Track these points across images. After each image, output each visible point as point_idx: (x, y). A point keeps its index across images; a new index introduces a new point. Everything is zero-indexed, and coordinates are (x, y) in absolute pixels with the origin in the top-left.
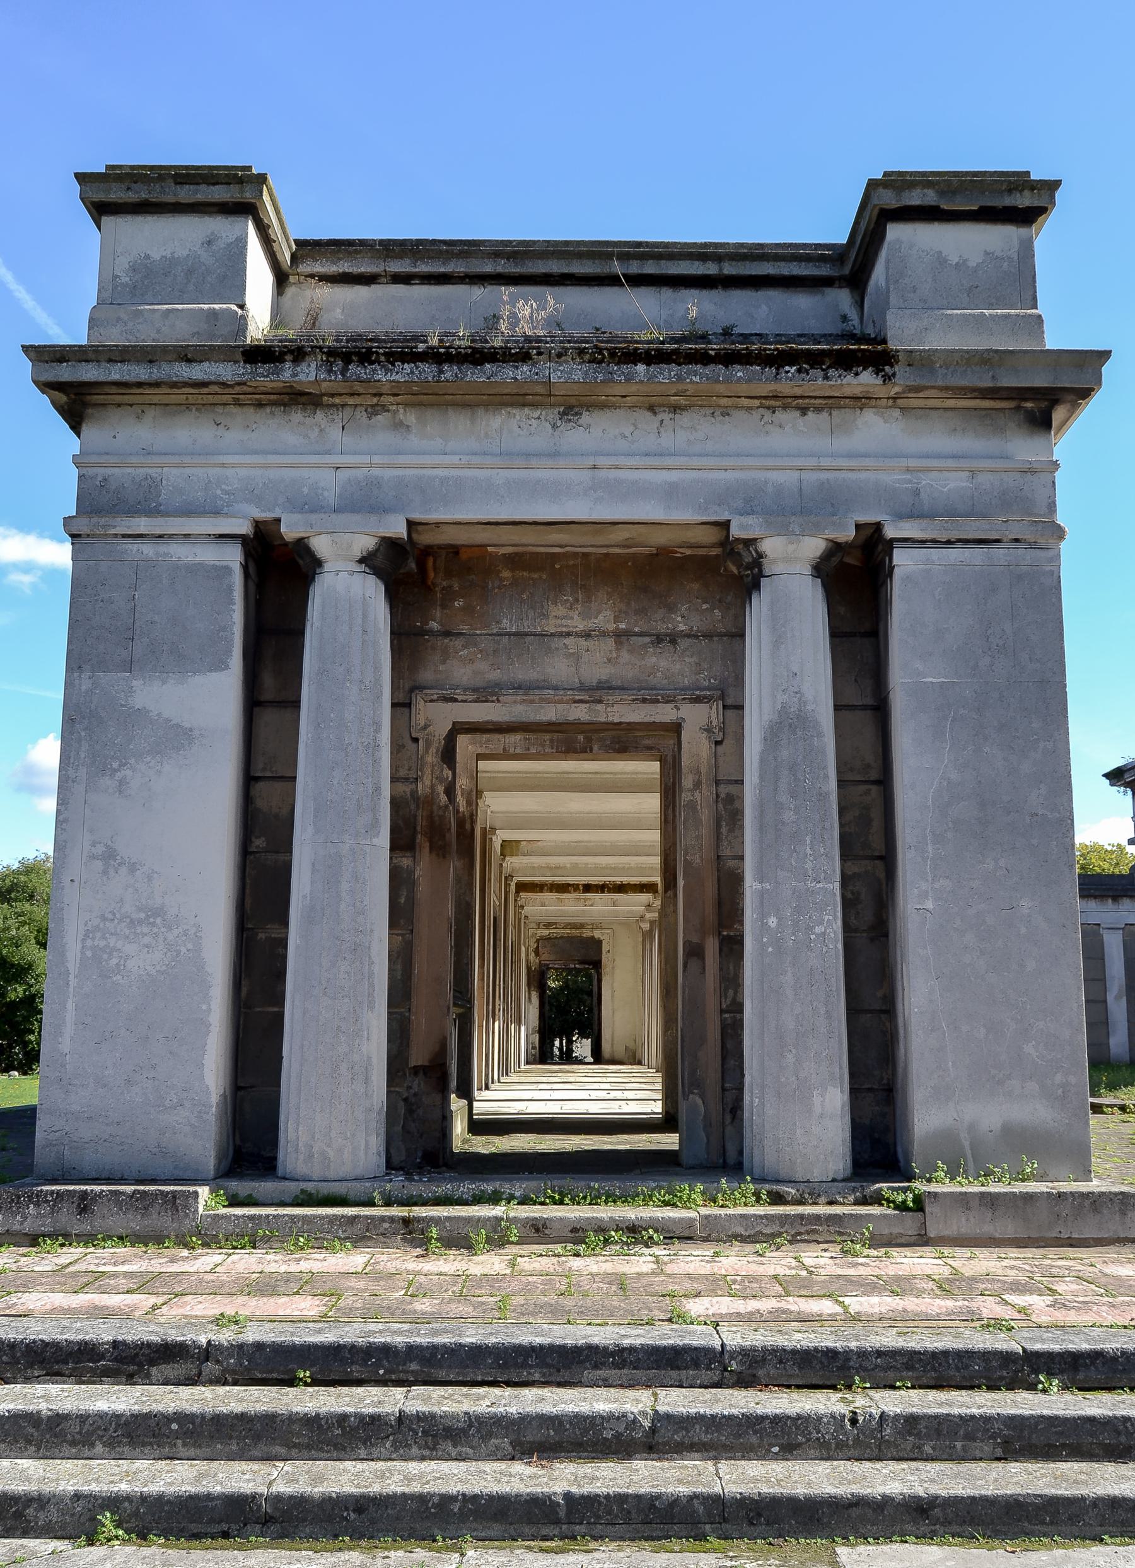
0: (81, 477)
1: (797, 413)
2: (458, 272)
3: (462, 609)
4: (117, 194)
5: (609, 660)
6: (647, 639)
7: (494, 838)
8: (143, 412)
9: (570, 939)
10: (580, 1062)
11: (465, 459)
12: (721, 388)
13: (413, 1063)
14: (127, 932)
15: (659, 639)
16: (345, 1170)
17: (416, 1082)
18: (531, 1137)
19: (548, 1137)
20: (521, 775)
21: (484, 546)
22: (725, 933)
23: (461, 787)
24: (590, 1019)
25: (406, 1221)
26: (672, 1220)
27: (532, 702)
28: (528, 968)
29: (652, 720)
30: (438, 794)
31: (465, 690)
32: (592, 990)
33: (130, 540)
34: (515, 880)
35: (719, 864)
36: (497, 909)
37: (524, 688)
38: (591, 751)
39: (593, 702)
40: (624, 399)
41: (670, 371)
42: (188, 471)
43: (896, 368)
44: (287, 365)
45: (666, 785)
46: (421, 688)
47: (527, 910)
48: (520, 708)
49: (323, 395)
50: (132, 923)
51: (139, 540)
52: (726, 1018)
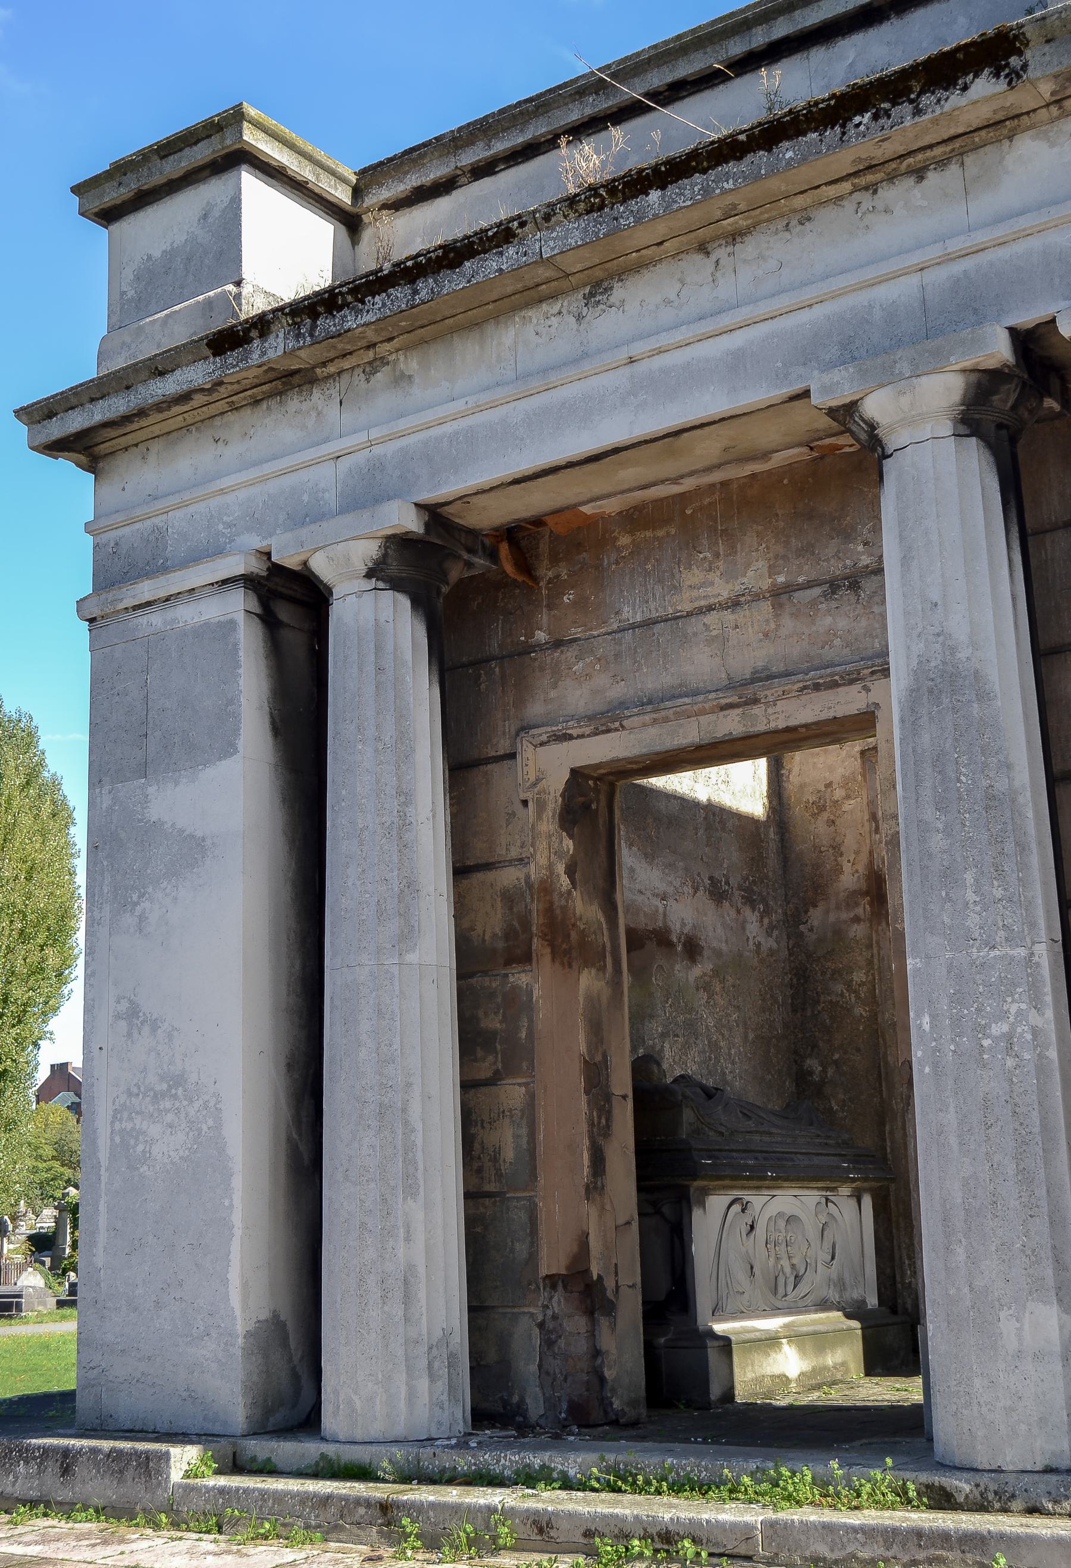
0: (96, 546)
1: (911, 181)
2: (542, 135)
3: (574, 604)
4: (113, 195)
5: (766, 635)
6: (817, 591)
8: (148, 449)
11: (472, 400)
12: (776, 185)
14: (151, 1109)
15: (833, 586)
16: (376, 1429)
21: (573, 507)
25: (385, 1507)
26: (720, 1525)
27: (666, 720)
29: (831, 714)
30: (558, 876)
33: (139, 612)
37: (651, 702)
39: (746, 703)
40: (662, 247)
41: (692, 186)
42: (191, 509)
43: (1028, 54)
44: (256, 343)
46: (525, 728)
48: (653, 731)
49: (314, 367)
50: (157, 1097)
51: (148, 609)
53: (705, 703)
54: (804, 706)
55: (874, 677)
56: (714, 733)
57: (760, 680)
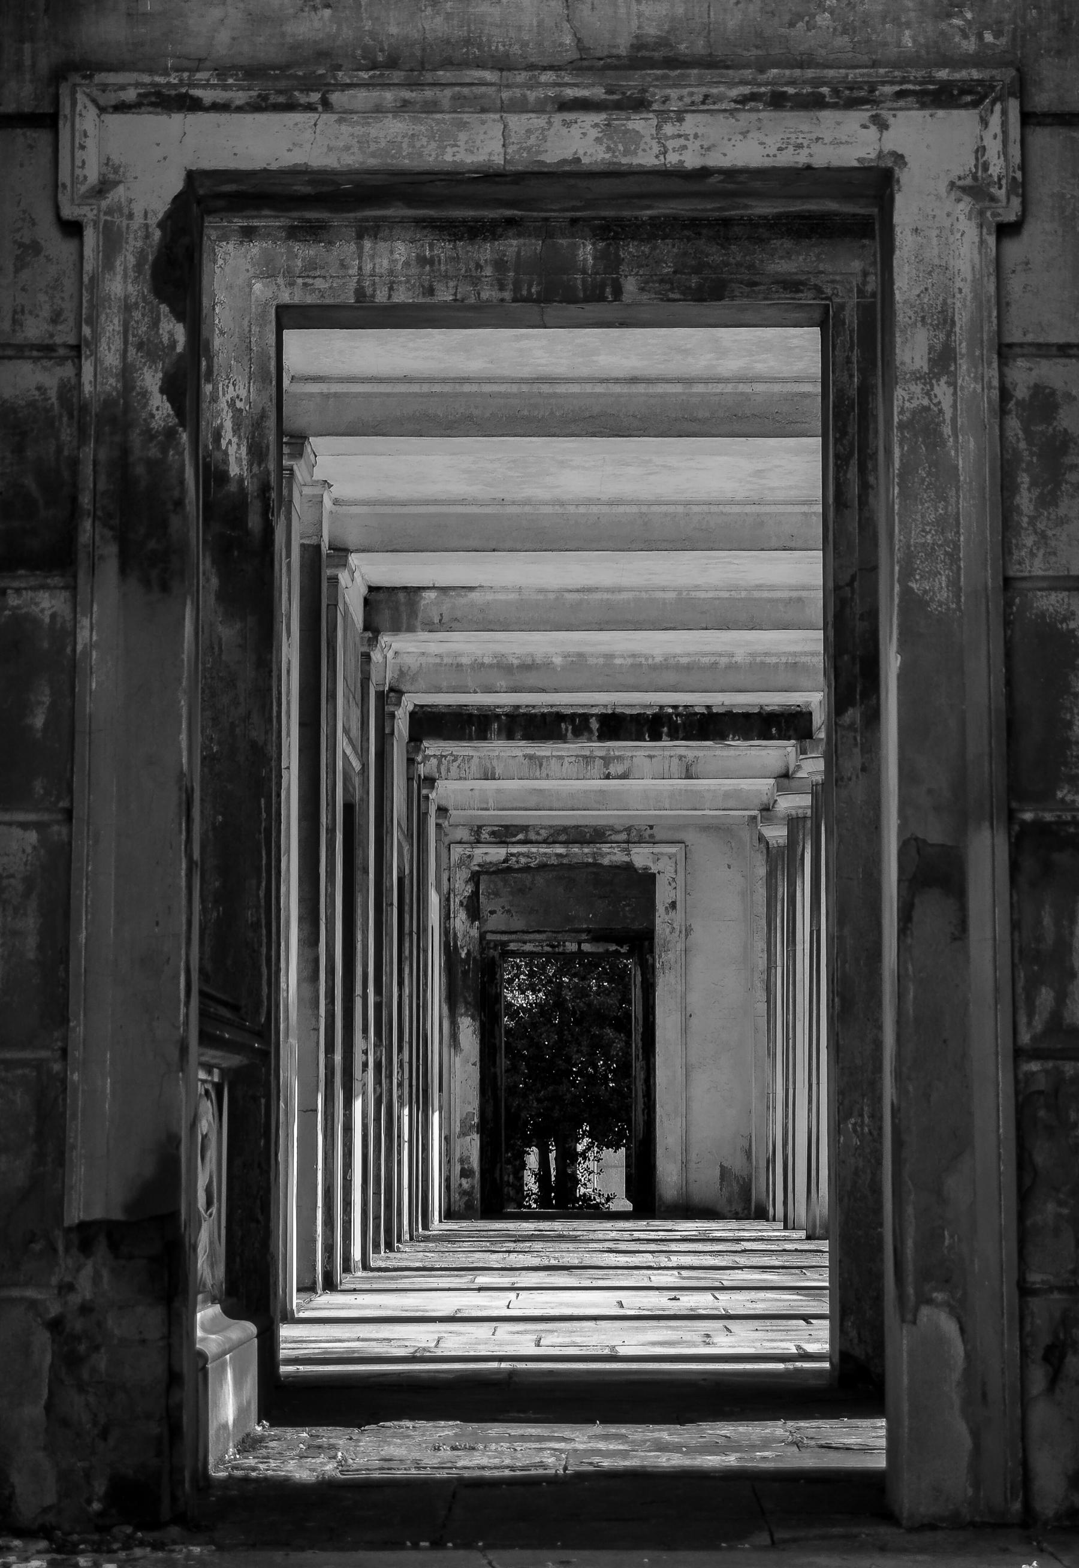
7: (343, 577)
9: (564, 871)
10: (594, 1211)
13: (75, 1213)
17: (88, 1270)
18: (446, 1430)
19: (495, 1429)
20: (415, 388)
22: (1028, 816)
23: (232, 404)
24: (623, 1096)
27: (431, 107)
28: (450, 950)
29: (801, 159)
30: (145, 394)
31: (222, 71)
32: (628, 1015)
34: (409, 702)
35: (1008, 604)
36: (357, 781)
38: (618, 292)
39: (618, 106)
45: (840, 395)
47: (446, 791)
48: (395, 127)
52: (1031, 1076)
53: (531, 88)
54: (745, 134)
55: (901, 103)
56: (538, 153)
57: (652, 64)
